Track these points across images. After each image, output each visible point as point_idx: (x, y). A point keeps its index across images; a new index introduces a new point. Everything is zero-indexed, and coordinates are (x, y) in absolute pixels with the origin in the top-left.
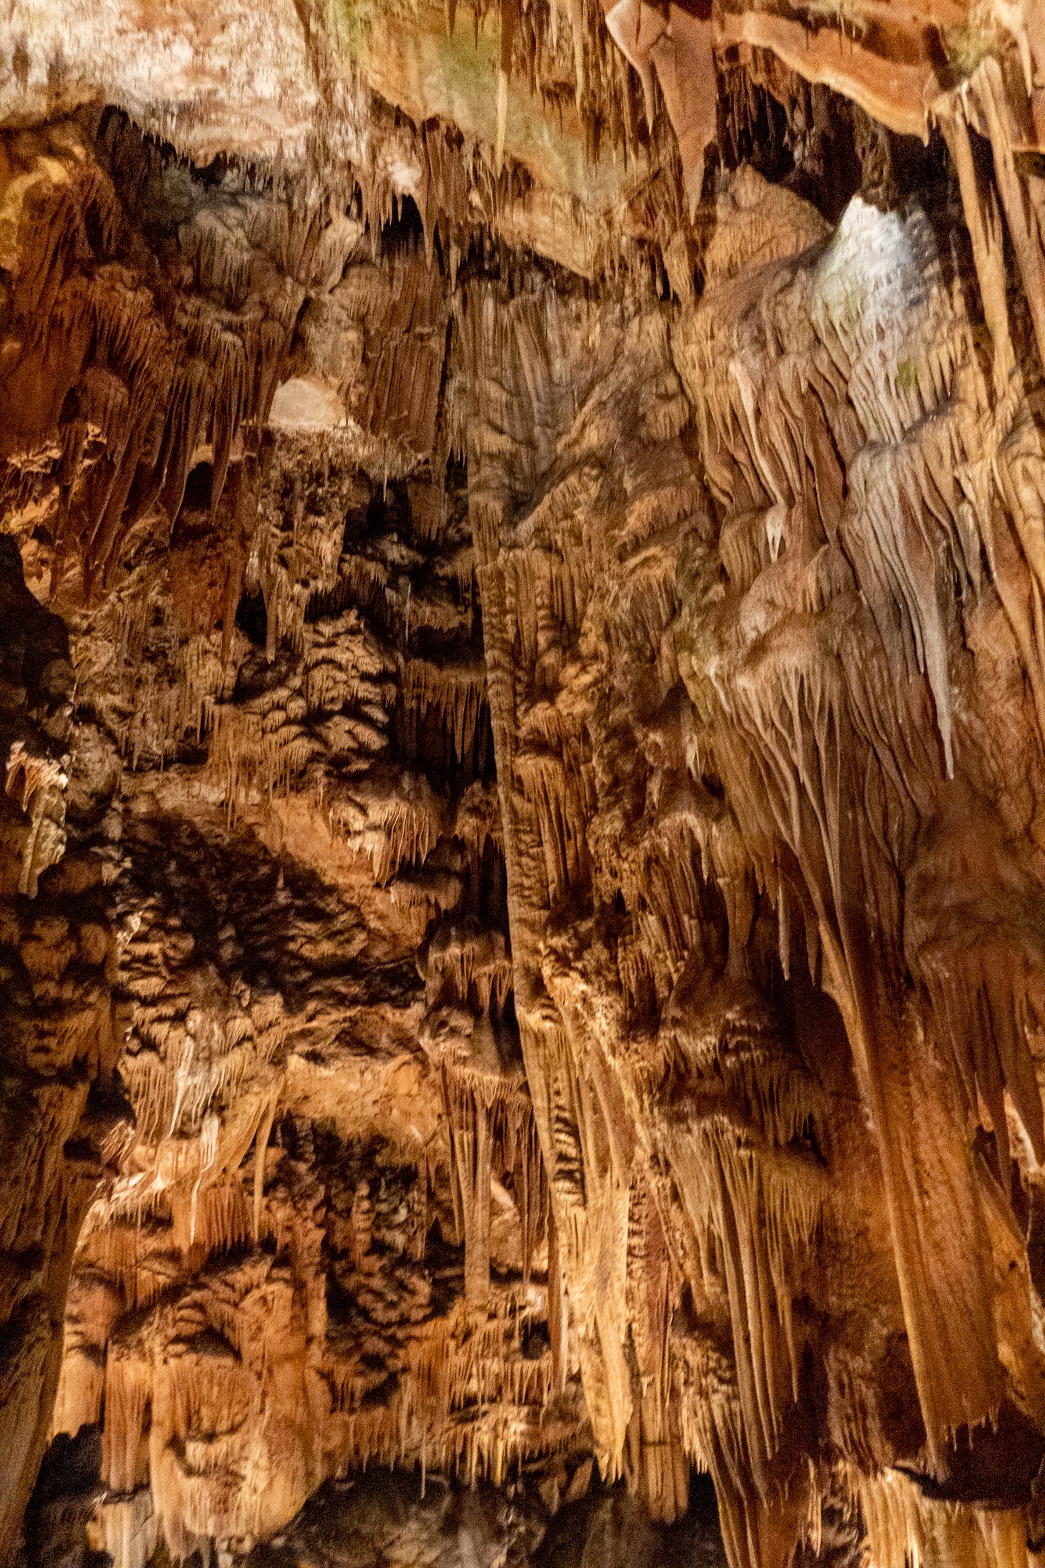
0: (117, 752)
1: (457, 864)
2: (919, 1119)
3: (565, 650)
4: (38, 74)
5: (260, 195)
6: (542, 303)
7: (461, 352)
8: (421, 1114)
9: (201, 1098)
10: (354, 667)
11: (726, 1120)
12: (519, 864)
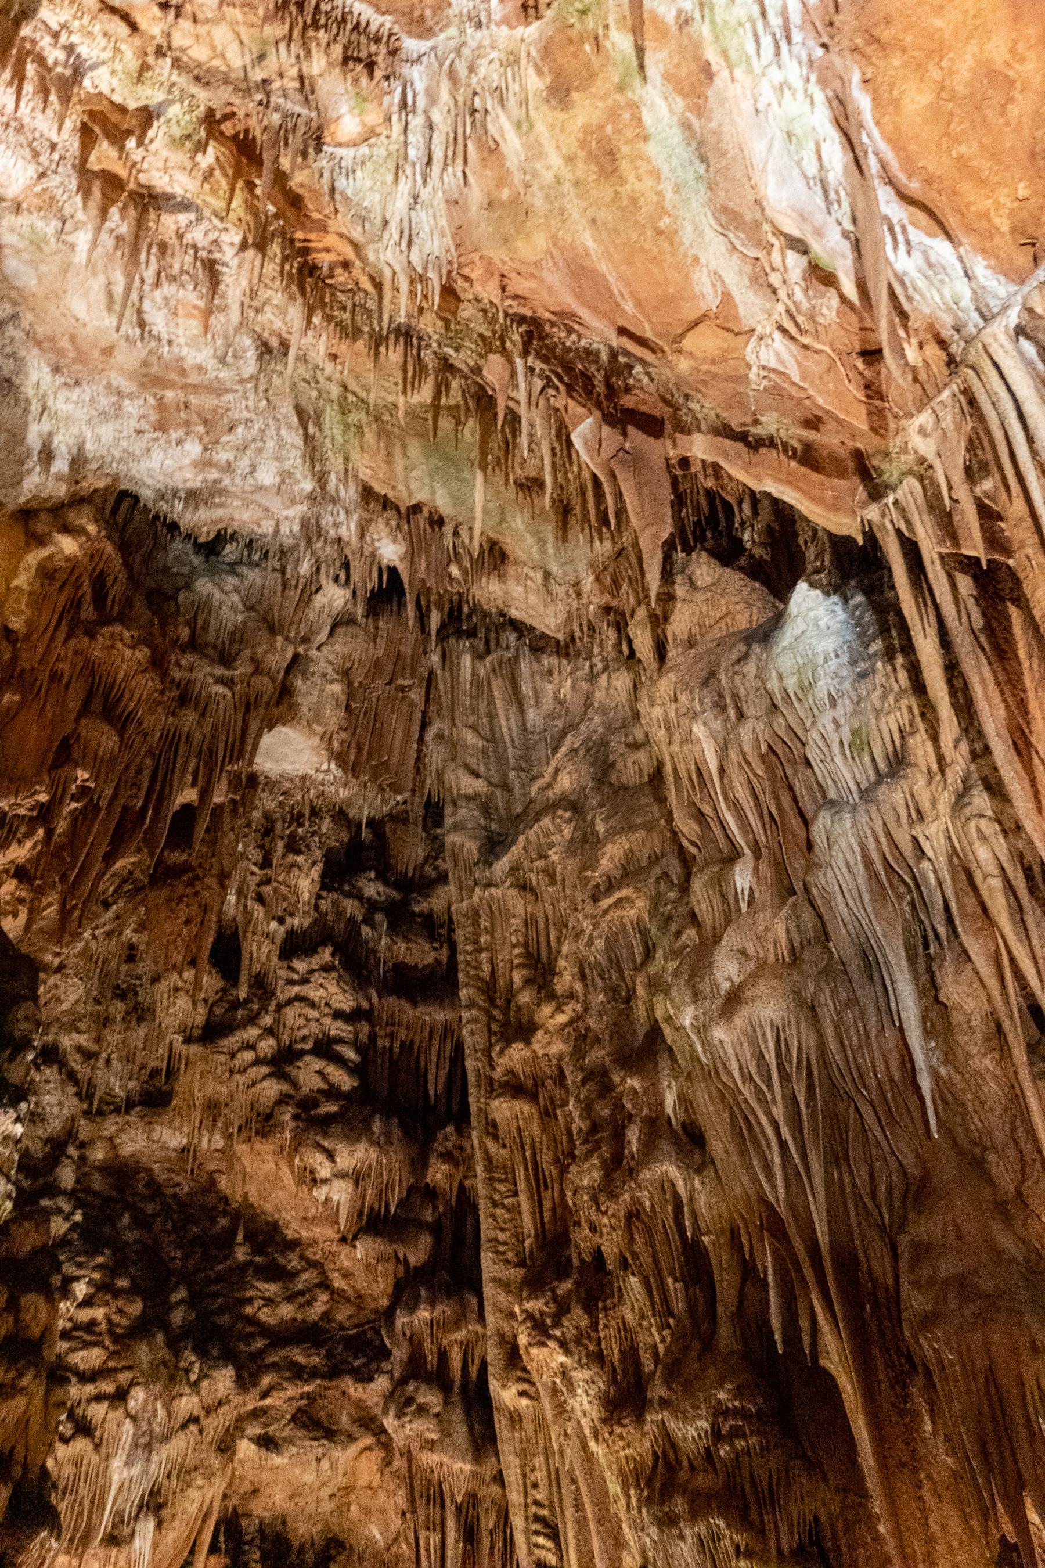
0: (78, 1094)
1: (428, 1215)
2: (935, 1528)
3: (540, 988)
4: (61, 465)
5: (257, 565)
6: (517, 658)
7: (440, 703)
8: (383, 1511)
9: (136, 1494)
10: (327, 1004)
11: (722, 1524)
12: (493, 1216)
